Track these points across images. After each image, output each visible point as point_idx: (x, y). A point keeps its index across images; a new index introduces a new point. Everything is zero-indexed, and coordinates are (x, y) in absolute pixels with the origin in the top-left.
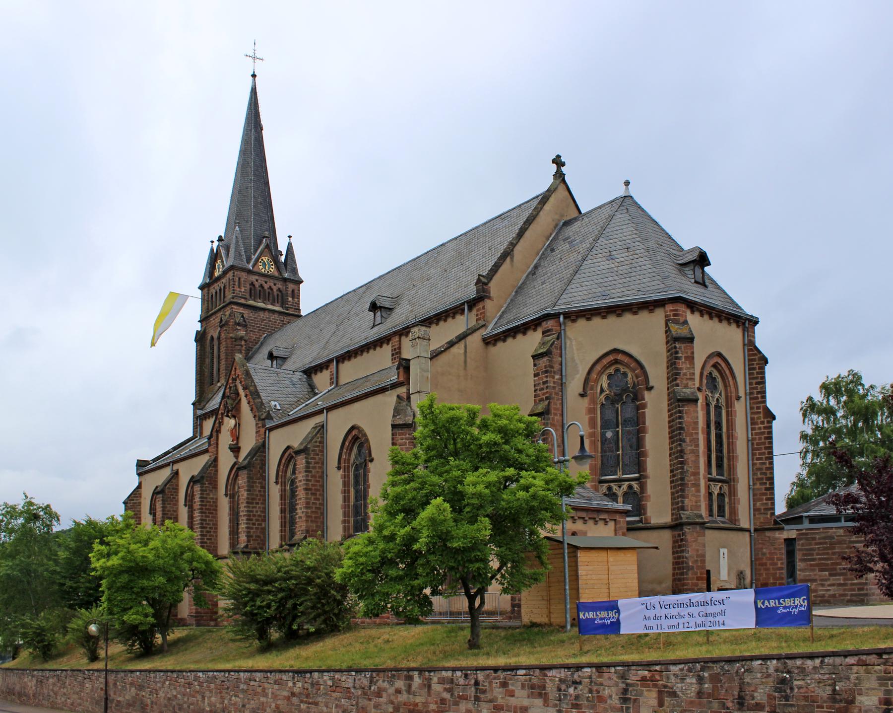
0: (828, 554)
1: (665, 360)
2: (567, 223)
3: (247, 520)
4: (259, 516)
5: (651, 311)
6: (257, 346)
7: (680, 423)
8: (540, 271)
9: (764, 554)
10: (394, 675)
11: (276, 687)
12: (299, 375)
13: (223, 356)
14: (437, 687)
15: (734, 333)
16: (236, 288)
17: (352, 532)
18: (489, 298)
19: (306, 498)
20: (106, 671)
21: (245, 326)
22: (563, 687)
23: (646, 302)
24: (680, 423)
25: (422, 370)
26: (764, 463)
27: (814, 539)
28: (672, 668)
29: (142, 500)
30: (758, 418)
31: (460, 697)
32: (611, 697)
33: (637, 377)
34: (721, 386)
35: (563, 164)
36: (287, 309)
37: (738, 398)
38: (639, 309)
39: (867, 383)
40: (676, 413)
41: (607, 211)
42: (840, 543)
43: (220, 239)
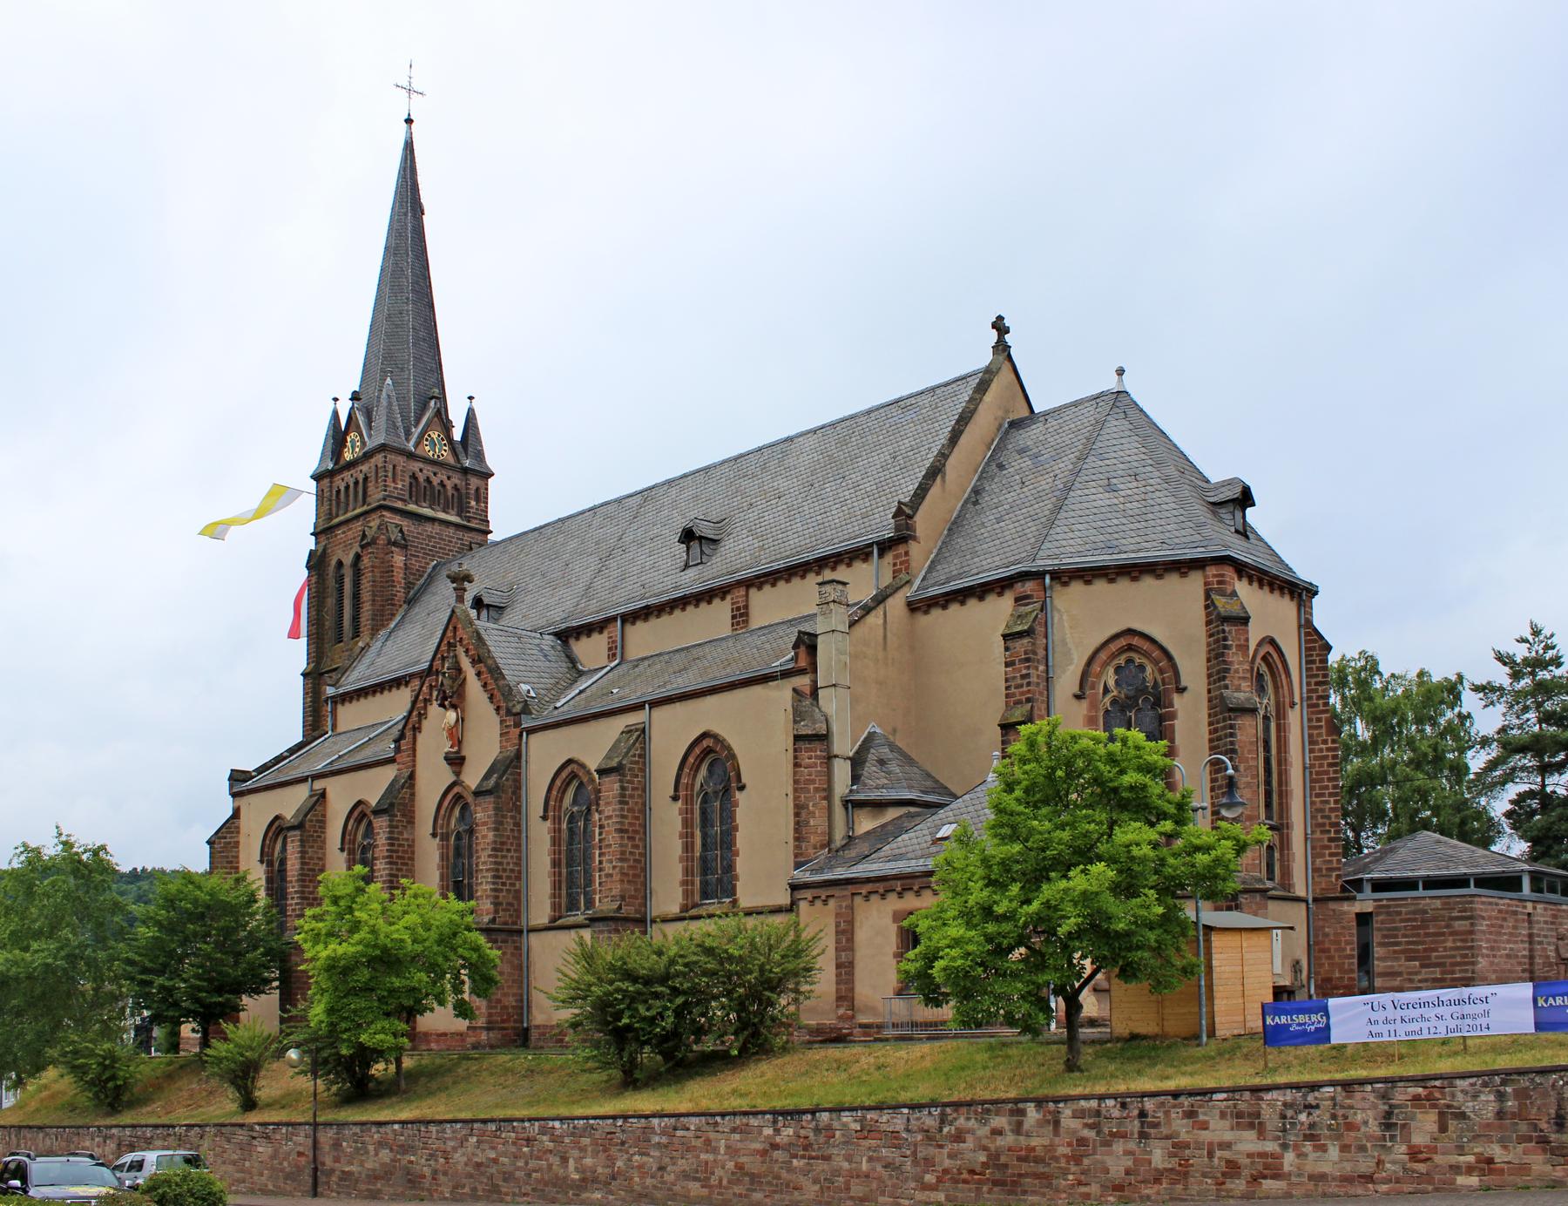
0: (1418, 935)
1: (1204, 649)
2: (1015, 425)
3: (495, 877)
4: (512, 871)
5: (1184, 575)
6: (422, 581)
7: (1232, 743)
8: (985, 499)
9: (1327, 935)
10: (988, 1111)
11: (737, 1137)
12: (549, 640)
13: (366, 596)
14: (1068, 1121)
15: (1285, 608)
16: (390, 480)
17: (697, 898)
18: (914, 538)
19: (621, 845)
20: (315, 1125)
21: (405, 547)
22: (1290, 1113)
23: (1179, 562)
24: (1232, 743)
25: (840, 652)
26: (1327, 802)
27: (1399, 913)
28: (1458, 1082)
29: (242, 839)
30: (1319, 735)
31: (1112, 1135)
32: (1366, 1123)
33: (1161, 671)
34: (1270, 690)
35: (1007, 331)
36: (469, 519)
37: (1293, 705)
38: (1166, 570)
39: (1386, 669)
40: (1224, 728)
41: (1089, 413)
42: (1435, 919)
43: (355, 397)
